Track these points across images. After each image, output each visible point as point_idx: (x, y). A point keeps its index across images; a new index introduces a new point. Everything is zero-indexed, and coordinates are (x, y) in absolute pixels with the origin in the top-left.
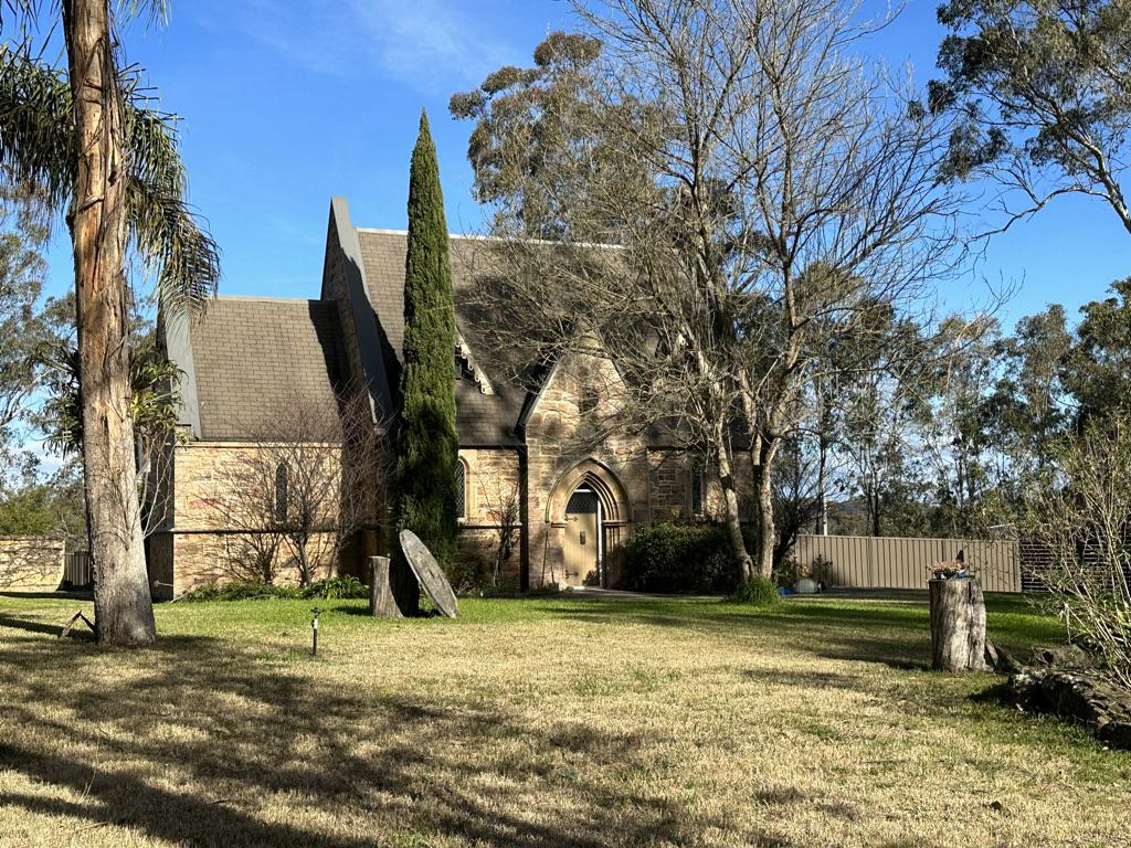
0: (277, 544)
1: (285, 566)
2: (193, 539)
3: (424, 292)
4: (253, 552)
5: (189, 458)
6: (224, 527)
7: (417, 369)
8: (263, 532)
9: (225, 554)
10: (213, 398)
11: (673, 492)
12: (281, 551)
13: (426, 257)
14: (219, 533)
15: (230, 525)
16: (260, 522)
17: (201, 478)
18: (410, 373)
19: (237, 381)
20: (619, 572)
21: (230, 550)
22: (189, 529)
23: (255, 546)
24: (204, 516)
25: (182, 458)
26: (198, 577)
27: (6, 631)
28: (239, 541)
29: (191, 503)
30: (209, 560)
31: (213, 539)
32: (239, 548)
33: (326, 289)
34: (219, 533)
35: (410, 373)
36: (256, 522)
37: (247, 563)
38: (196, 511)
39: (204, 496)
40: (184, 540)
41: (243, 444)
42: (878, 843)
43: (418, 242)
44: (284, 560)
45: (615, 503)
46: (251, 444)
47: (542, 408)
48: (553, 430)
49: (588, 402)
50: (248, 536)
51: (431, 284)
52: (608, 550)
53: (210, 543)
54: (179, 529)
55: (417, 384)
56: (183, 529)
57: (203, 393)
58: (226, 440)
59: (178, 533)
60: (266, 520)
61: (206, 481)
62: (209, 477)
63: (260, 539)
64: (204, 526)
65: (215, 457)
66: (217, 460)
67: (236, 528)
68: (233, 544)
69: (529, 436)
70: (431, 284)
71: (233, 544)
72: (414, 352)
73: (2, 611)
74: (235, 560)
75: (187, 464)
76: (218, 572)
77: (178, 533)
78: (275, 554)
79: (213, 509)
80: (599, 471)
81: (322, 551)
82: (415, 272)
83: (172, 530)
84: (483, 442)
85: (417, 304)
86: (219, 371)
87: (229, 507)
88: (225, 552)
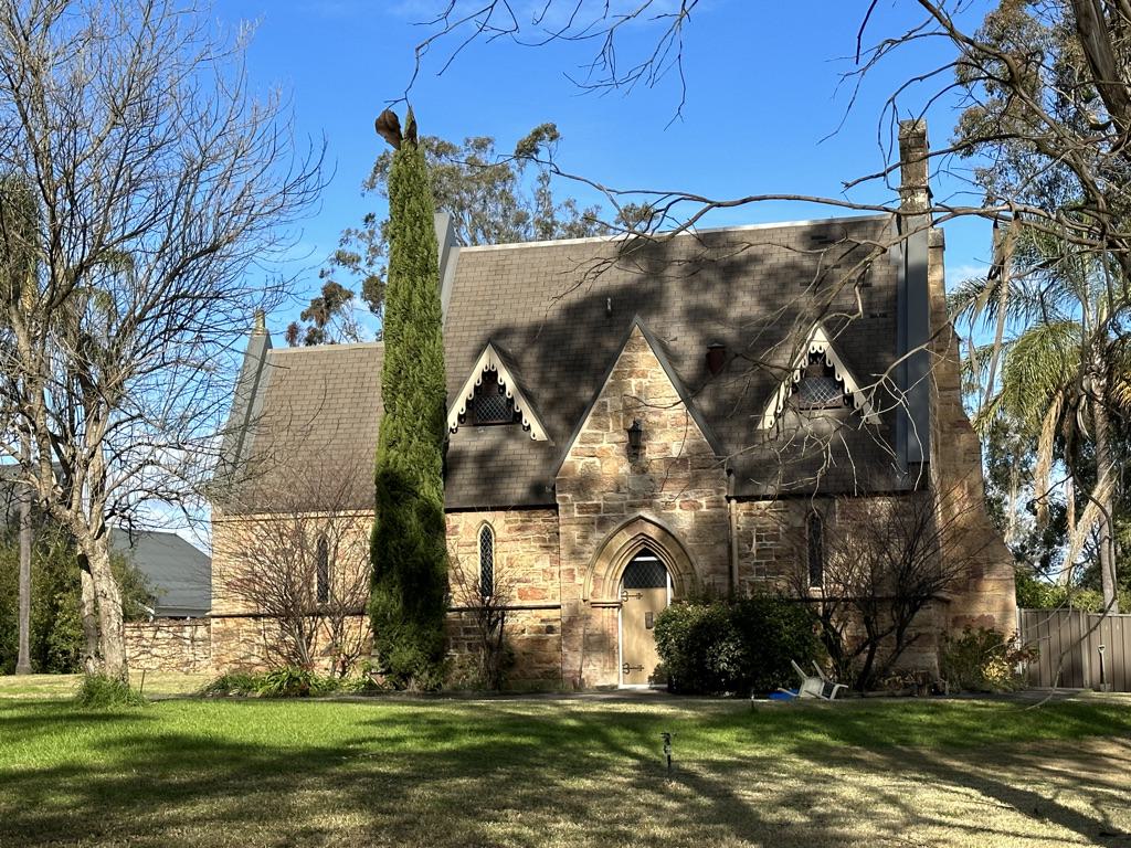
0: (316, 629)
2: (231, 623)
9: (263, 642)
11: (777, 557)
12: (320, 636)
21: (267, 636)
22: (224, 613)
26: (234, 666)
27: (1130, 768)
30: (244, 647)
31: (250, 624)
33: (161, 536)
37: (285, 650)
40: (221, 625)
44: (323, 648)
47: (575, 458)
48: (584, 485)
49: (636, 439)
53: (245, 627)
54: (214, 613)
59: (214, 617)
68: (269, 629)
71: (269, 629)
74: (272, 648)
76: (255, 660)
77: (214, 617)
78: (313, 640)
80: (652, 531)
81: (363, 637)
84: (497, 501)
88: (262, 638)
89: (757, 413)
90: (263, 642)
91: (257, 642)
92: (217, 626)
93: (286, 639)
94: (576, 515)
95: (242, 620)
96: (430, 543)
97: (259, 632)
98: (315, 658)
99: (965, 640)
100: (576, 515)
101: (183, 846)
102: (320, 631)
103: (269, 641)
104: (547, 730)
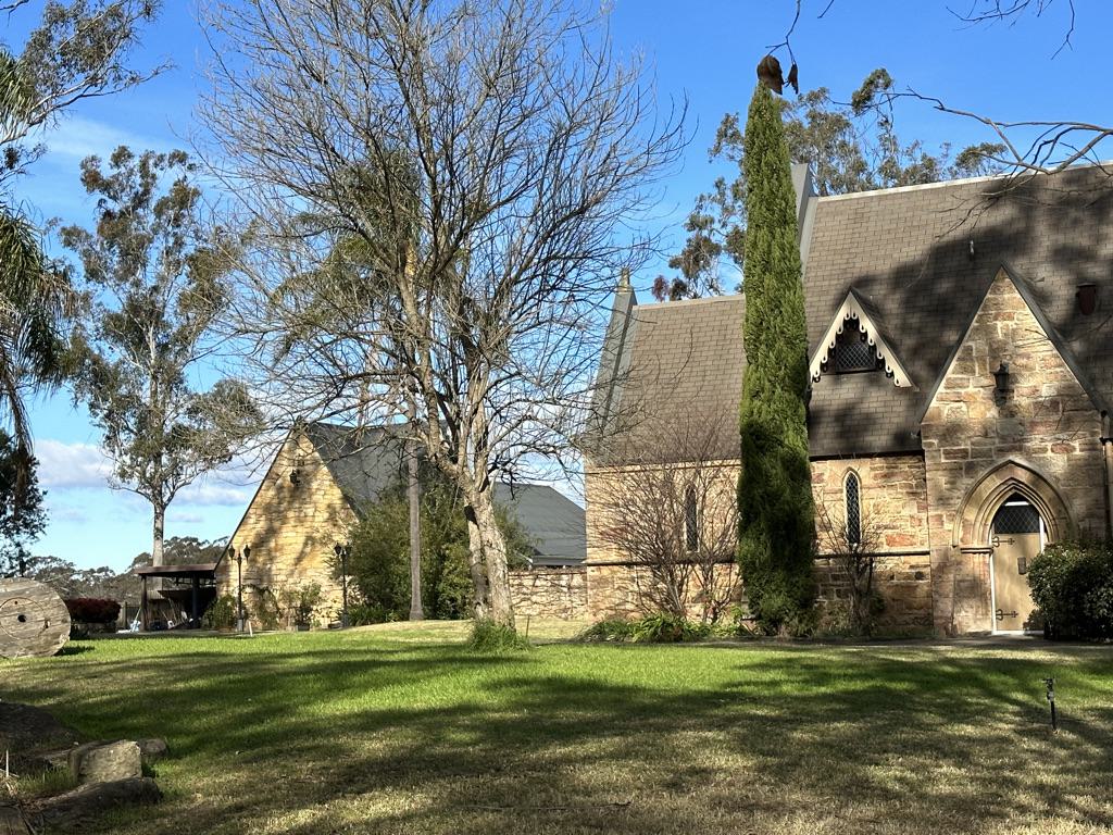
12: (690, 584)
31: (623, 572)
37: (657, 597)
44: (694, 595)
56: (599, 561)
68: (642, 577)
71: (642, 577)
78: (685, 587)
88: (635, 586)
91: (631, 589)
94: (943, 461)
95: (616, 568)
96: (796, 491)
97: (633, 580)
100: (943, 461)
103: (643, 588)
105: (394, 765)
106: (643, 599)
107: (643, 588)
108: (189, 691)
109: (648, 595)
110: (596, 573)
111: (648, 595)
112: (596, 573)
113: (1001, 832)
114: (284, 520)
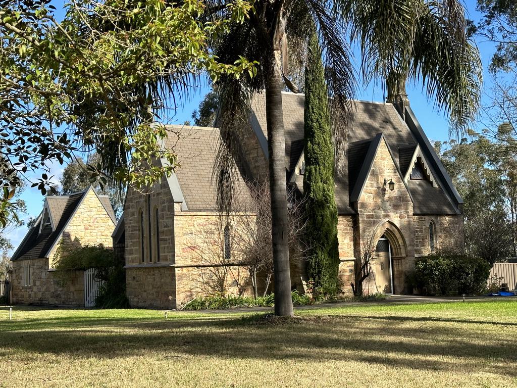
1: (231, 286)
3: (320, 124)
4: (215, 278)
5: (181, 222)
6: (200, 263)
7: (318, 169)
8: (220, 266)
9: (201, 280)
10: (187, 186)
12: (229, 276)
13: (319, 103)
14: (198, 267)
15: (203, 262)
16: (218, 260)
17: (187, 234)
18: (314, 171)
19: (197, 176)
20: (403, 285)
21: (203, 277)
23: (215, 274)
24: (190, 257)
25: (178, 222)
28: (207, 271)
29: (183, 249)
31: (195, 271)
32: (207, 276)
34: (198, 267)
35: (314, 171)
36: (217, 261)
37: (211, 284)
38: (186, 254)
39: (189, 245)
41: (209, 214)
42: (338, 386)
43: (314, 95)
44: (230, 282)
45: (399, 246)
46: (213, 214)
50: (212, 268)
51: (323, 120)
52: (395, 273)
55: (318, 178)
56: (181, 265)
57: (181, 183)
58: (200, 211)
60: (221, 259)
61: (190, 235)
62: (191, 233)
63: (218, 269)
64: (189, 263)
65: (194, 221)
66: (195, 223)
67: (206, 264)
68: (204, 273)
69: (360, 208)
70: (323, 120)
71: (204, 273)
72: (315, 159)
73: (513, 365)
75: (180, 225)
78: (226, 278)
79: (194, 252)
82: (313, 113)
83: (175, 265)
85: (316, 131)
86: (186, 170)
87: (202, 251)
88: (201, 278)
89: (247, 55)
90: (201, 280)
91: (199, 280)
92: (179, 272)
93: (213, 278)
94: (366, 219)
95: (191, 269)
96: (332, 223)
97: (200, 275)
98: (227, 288)
99: (279, 85)
100: (366, 219)
101: (241, 387)
102: (228, 274)
103: (205, 279)
104: (342, 298)
105: (389, 334)
106: (205, 285)
107: (205, 279)
108: (61, 327)
109: (207, 283)
110: (180, 272)
111: (207, 283)
112: (180, 272)
113: (404, 385)
114: (34, 220)
